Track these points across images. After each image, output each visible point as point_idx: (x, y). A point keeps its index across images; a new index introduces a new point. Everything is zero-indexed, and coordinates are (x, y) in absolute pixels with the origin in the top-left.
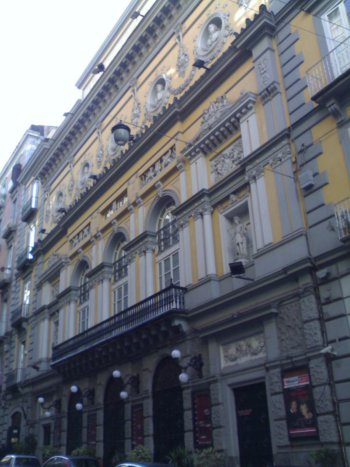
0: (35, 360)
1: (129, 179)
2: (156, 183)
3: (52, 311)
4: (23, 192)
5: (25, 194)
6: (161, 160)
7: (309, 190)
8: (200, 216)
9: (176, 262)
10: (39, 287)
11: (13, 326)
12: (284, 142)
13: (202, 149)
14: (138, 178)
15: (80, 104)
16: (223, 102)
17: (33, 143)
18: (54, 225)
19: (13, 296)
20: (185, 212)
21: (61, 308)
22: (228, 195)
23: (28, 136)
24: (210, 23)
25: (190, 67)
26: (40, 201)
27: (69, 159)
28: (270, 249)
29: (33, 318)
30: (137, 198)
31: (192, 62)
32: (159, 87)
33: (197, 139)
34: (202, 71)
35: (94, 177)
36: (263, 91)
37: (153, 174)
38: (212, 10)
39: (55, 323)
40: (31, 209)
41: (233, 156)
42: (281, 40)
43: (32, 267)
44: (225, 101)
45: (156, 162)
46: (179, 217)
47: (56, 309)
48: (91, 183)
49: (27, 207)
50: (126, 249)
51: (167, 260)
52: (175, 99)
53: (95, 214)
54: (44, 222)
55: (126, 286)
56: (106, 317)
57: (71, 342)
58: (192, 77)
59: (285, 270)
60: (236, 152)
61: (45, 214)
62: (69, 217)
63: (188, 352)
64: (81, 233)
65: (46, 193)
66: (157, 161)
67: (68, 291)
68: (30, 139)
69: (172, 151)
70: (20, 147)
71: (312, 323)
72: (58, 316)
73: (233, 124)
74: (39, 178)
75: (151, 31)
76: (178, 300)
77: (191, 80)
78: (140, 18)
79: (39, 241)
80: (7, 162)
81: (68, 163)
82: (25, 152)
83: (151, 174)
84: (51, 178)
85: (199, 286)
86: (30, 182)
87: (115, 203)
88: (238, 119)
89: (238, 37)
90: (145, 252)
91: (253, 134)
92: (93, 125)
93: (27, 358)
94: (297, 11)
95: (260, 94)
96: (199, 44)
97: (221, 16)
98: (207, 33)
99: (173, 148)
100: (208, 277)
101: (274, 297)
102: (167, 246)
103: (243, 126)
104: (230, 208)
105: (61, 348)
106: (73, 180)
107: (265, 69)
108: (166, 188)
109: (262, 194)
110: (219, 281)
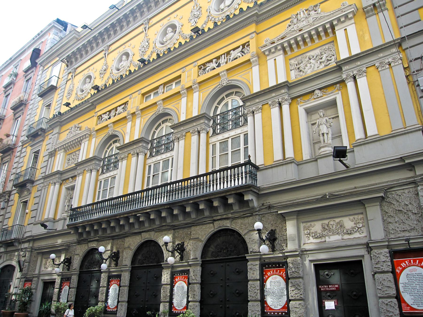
4: (40, 72)
5: (42, 74)
6: (116, 109)
8: (136, 155)
9: (112, 182)
12: (394, 50)
13: (284, 49)
17: (56, 34)
20: (126, 150)
23: (54, 26)
29: (42, 181)
30: (194, 83)
32: (124, 57)
34: (68, 108)
35: (96, 88)
37: (109, 117)
45: (112, 109)
46: (176, 131)
50: (173, 127)
51: (224, 143)
55: (246, 136)
59: (402, 159)
61: (66, 92)
68: (54, 30)
70: (41, 35)
82: (47, 40)
98: (165, 33)
101: (383, 183)
102: (108, 170)
106: (103, 68)
108: (116, 130)
110: (298, 165)
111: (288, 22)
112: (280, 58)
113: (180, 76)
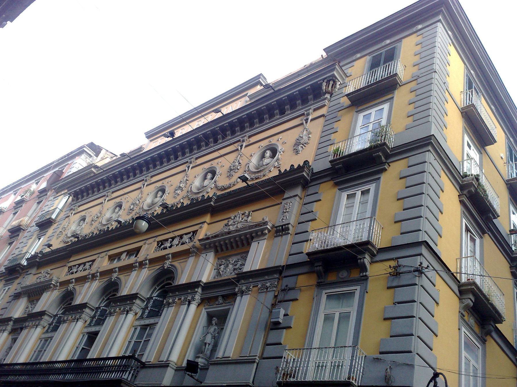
1: (109, 250)
2: (167, 255)
6: (181, 237)
7: (276, 326)
10: (17, 296)
12: (276, 276)
15: (138, 153)
16: (248, 218)
18: (62, 245)
21: (26, 327)
22: (218, 296)
25: (236, 176)
26: (62, 215)
27: (146, 177)
28: (227, 362)
31: (240, 174)
32: (160, 193)
33: (216, 236)
35: (119, 222)
36: (279, 226)
38: (273, 140)
39: (12, 339)
41: (236, 265)
42: (309, 193)
44: (250, 218)
47: (21, 326)
48: (115, 225)
52: (215, 194)
54: (55, 238)
56: (62, 358)
57: (18, 367)
58: (236, 183)
60: (240, 263)
62: (81, 246)
64: (82, 266)
65: (71, 211)
66: (178, 236)
67: (42, 313)
69: (193, 235)
72: (19, 334)
73: (247, 239)
74: (72, 195)
75: (223, 130)
76: (132, 372)
77: (234, 185)
78: (219, 115)
79: (41, 252)
80: (9, 186)
81: (104, 196)
83: (168, 245)
84: (234, 138)
86: (63, 192)
88: (252, 238)
89: (281, 175)
91: (258, 256)
95: (276, 227)
96: (254, 161)
97: (279, 149)
99: (195, 232)
100: (168, 362)
103: (254, 245)
104: (214, 309)
107: (288, 210)
109: (244, 309)
111: (226, 222)
112: (211, 256)
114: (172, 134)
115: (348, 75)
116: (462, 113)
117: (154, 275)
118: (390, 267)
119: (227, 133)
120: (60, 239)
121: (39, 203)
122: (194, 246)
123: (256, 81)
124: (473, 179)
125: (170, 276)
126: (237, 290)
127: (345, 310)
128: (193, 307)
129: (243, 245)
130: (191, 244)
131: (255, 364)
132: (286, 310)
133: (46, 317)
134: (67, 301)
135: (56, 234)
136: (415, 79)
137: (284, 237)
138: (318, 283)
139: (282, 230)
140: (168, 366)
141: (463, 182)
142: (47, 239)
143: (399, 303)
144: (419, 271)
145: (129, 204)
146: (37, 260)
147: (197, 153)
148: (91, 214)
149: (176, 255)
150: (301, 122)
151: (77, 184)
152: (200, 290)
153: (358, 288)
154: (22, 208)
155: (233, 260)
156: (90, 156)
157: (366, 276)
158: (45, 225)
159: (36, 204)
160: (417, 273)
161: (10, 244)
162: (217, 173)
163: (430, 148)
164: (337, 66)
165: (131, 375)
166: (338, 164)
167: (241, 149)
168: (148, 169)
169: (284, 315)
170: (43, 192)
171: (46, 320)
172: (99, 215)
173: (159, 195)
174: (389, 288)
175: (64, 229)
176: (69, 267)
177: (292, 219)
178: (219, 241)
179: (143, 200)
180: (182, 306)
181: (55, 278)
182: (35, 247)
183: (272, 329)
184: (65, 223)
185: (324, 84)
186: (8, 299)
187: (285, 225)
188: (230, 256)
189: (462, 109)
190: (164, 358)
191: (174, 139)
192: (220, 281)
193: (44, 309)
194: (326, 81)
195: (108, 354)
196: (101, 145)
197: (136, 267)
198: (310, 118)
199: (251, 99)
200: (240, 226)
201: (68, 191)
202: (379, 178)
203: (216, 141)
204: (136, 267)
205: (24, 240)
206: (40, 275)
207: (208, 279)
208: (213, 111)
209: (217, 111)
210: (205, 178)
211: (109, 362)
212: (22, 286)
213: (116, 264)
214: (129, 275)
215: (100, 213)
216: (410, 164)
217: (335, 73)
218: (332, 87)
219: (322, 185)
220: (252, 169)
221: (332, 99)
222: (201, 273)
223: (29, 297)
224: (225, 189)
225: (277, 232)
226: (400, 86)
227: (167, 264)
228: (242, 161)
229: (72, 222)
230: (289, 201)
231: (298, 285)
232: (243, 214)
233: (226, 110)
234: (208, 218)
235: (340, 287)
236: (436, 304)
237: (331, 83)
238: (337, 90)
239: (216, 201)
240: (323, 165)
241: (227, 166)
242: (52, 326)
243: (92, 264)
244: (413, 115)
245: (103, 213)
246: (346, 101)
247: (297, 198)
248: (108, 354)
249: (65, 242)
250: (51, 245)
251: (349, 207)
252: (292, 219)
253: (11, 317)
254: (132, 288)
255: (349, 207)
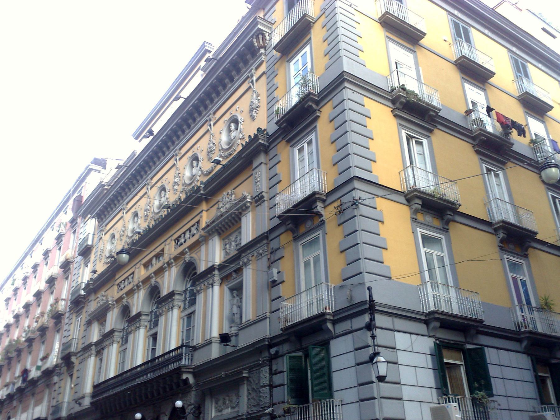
0: (80, 395)
3: (99, 348)
6: (190, 230)
7: (274, 284)
8: (211, 286)
10: (89, 323)
11: (63, 358)
12: (265, 242)
14: (173, 242)
15: (134, 159)
18: (106, 267)
19: (66, 327)
21: (105, 347)
22: (230, 271)
24: (231, 123)
26: (96, 239)
27: (175, 152)
32: (195, 163)
33: (213, 222)
36: (256, 197)
38: (233, 111)
40: (87, 245)
42: (271, 157)
43: (84, 303)
44: (233, 196)
49: (83, 244)
53: (138, 264)
54: (98, 261)
56: (139, 363)
63: (192, 402)
64: (126, 281)
67: (112, 332)
70: (82, 180)
71: (264, 389)
73: (237, 216)
75: (160, 147)
76: (187, 357)
78: (181, 101)
81: (173, 156)
83: (182, 240)
84: (214, 105)
85: (204, 346)
87: (154, 259)
88: (241, 213)
89: (245, 148)
90: (172, 308)
91: (249, 229)
92: (204, 116)
93: (73, 391)
94: (280, 139)
95: (254, 198)
99: (198, 222)
103: (243, 219)
104: (233, 283)
105: (103, 386)
107: (258, 179)
109: (250, 277)
111: (216, 206)
113: (163, 250)
114: (151, 132)
115: (273, 22)
116: (380, 23)
117: (181, 270)
118: (335, 208)
119: (240, 65)
120: (103, 261)
121: (74, 232)
122: (201, 236)
123: (203, 51)
124: (399, 91)
125: (192, 267)
126: (241, 264)
127: (316, 254)
128: (216, 288)
129: (237, 222)
130: (199, 234)
131: (268, 320)
132: (277, 268)
133: (116, 334)
134: (156, 296)
135: (97, 258)
136: (323, 11)
137: (262, 204)
138: (294, 238)
139: (259, 199)
140: (211, 343)
141: (392, 96)
142: (92, 265)
143: (347, 236)
144: (355, 203)
145: (143, 210)
146: (91, 287)
147: (179, 144)
148: (167, 181)
149: (192, 247)
150: (249, 86)
151: (94, 207)
152: (216, 272)
153: (320, 232)
154: (50, 258)
155: (233, 238)
156: (99, 171)
157: (323, 220)
158: (86, 252)
159: (72, 234)
160: (354, 206)
161: (67, 278)
162: (239, 120)
163: (346, 84)
164: (258, 20)
165: (187, 359)
166: (282, 124)
167: (211, 128)
168: (173, 143)
169: (278, 273)
170: (73, 221)
171: (117, 336)
172: (123, 229)
173: (163, 195)
174: (339, 225)
175: (102, 251)
176: (174, 240)
177: (264, 186)
178: (218, 225)
179: (152, 203)
180: (208, 290)
181: (110, 299)
182: (85, 275)
183: (272, 287)
184: (101, 245)
185: (255, 40)
186: (83, 328)
187: (259, 194)
188: (230, 235)
189: (380, 19)
190: (208, 337)
191: (155, 137)
192: (230, 258)
193: (138, 311)
194: (254, 37)
195: (169, 348)
196: (104, 157)
197: (165, 268)
198: (254, 78)
199: (205, 72)
200: (228, 206)
201: (91, 215)
202: (316, 127)
203: (232, 80)
204: (165, 268)
205: (76, 272)
206: (98, 299)
207: (220, 259)
208: (174, 100)
209: (177, 98)
210: (230, 131)
211: (173, 354)
212: (89, 313)
213: (152, 270)
214: (200, 250)
215: (124, 227)
216: (335, 105)
217: (260, 26)
218: (263, 41)
219: (278, 146)
220: (225, 147)
221: (267, 52)
222: (214, 258)
223: (98, 320)
224: (210, 173)
225: (256, 202)
226: (314, 23)
227: (187, 258)
228: (216, 140)
229: (127, 221)
230: (257, 170)
231: (282, 244)
232: (227, 194)
233: (186, 93)
234: (204, 206)
235: (308, 236)
236: (380, 223)
237: (260, 36)
238: (268, 42)
239: (205, 188)
240: (272, 128)
241: (246, 108)
242: (187, 302)
243: (133, 276)
244: (328, 53)
245: (129, 223)
246: (277, 55)
247: (263, 165)
248: (169, 348)
249: (107, 263)
250: (96, 271)
251: (302, 160)
252: (264, 186)
253: (213, 265)
254: (168, 288)
255: (302, 160)
